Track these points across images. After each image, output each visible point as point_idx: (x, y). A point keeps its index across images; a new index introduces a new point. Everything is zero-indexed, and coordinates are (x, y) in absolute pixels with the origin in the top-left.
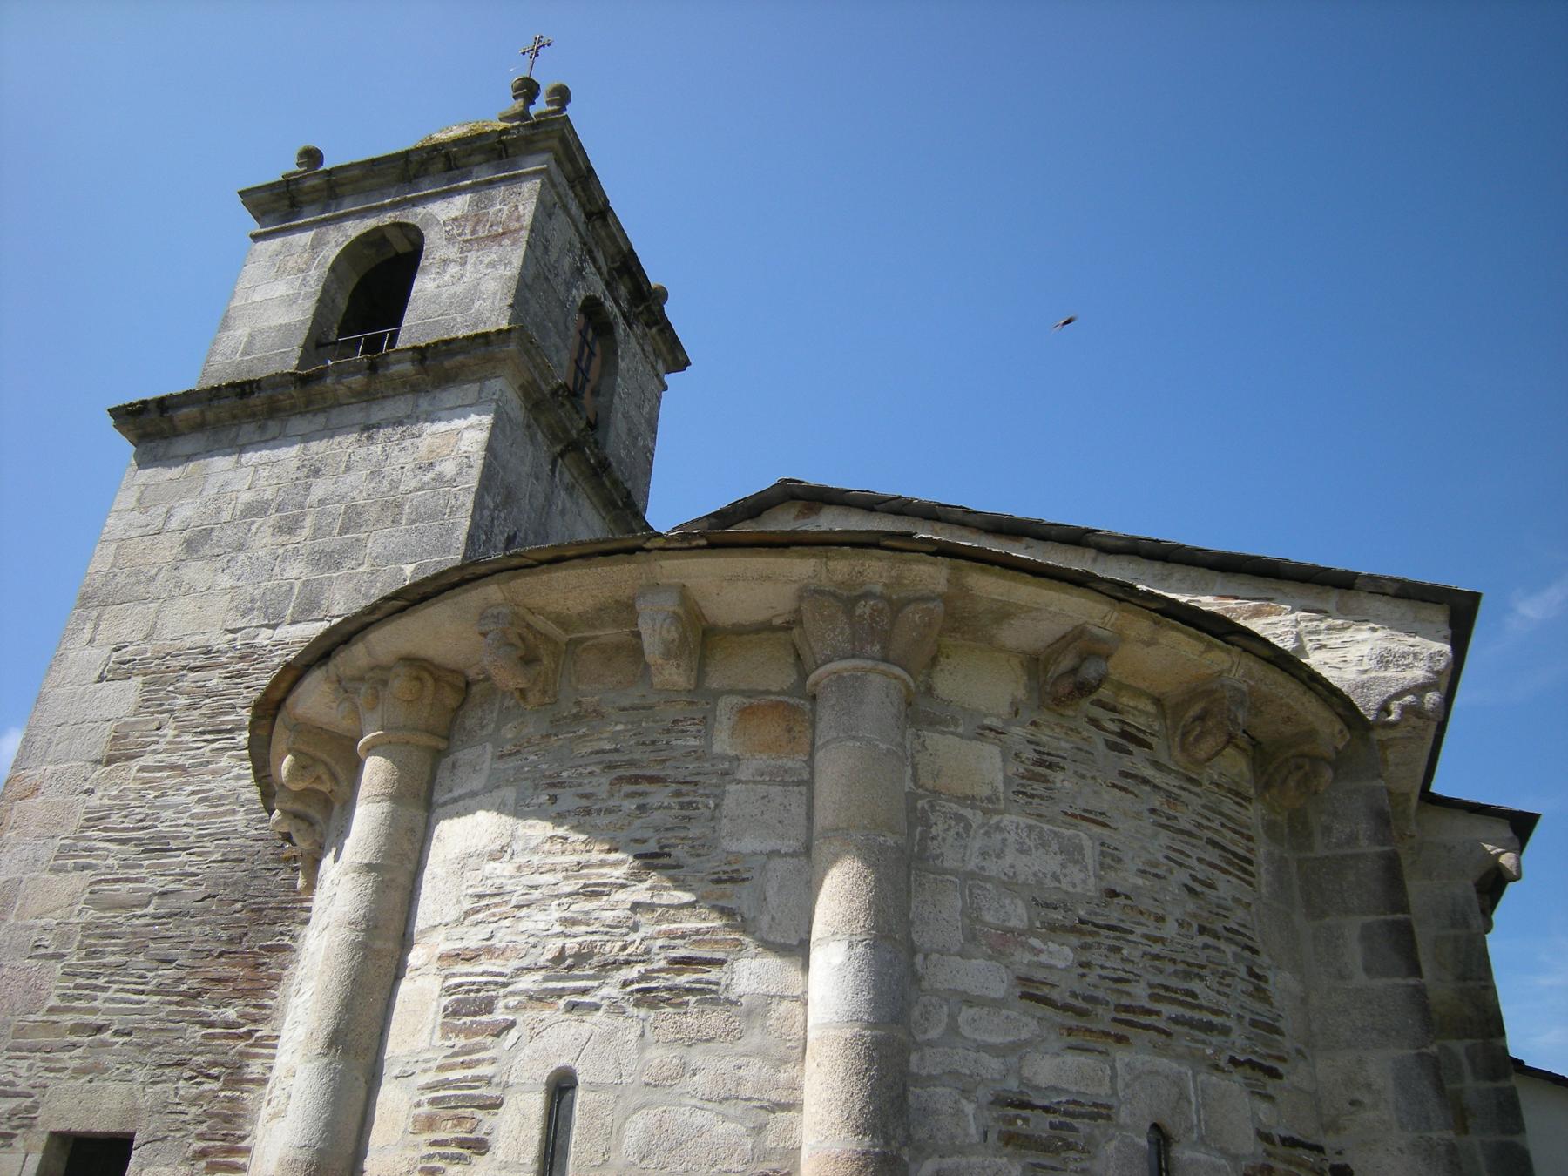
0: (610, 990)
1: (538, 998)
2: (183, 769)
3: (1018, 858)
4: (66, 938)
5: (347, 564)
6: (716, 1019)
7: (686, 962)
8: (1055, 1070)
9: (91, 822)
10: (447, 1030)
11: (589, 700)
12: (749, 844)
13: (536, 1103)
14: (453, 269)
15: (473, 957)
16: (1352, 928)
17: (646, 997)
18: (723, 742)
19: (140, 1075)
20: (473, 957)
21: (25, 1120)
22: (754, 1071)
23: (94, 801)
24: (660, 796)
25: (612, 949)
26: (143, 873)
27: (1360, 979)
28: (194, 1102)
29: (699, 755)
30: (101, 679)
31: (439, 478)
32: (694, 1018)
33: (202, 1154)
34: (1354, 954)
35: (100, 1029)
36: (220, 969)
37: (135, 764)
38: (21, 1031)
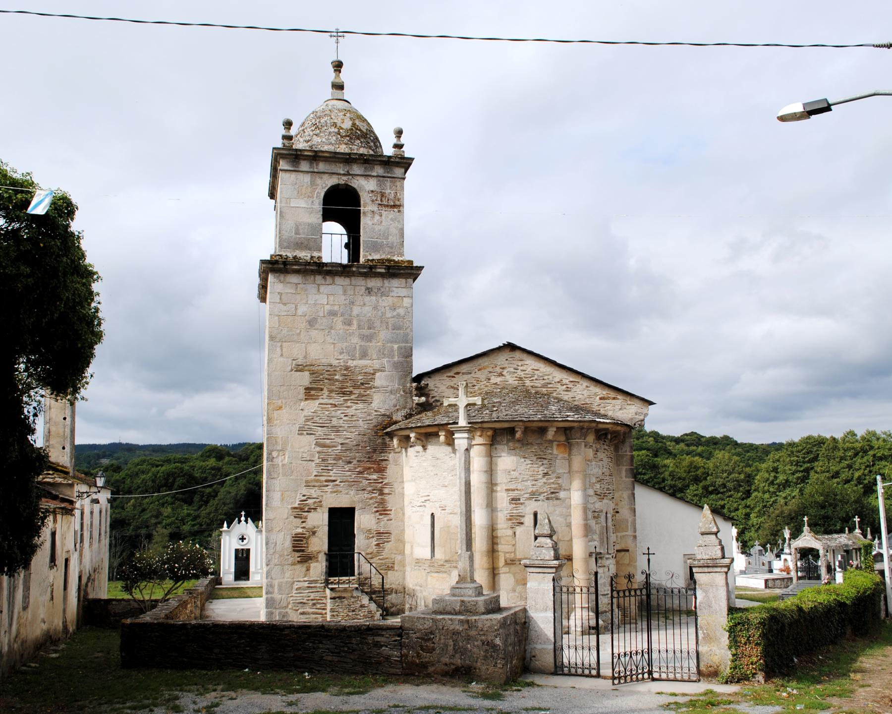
0: (541, 497)
1: (530, 499)
2: (335, 406)
3: (596, 470)
4: (313, 456)
5: (374, 341)
6: (558, 502)
7: (553, 493)
8: (598, 505)
9: (307, 420)
10: (510, 503)
11: (530, 441)
12: (561, 471)
13: (532, 517)
14: (377, 217)
15: (513, 490)
16: (624, 468)
17: (548, 499)
18: (555, 452)
19: (352, 493)
20: (513, 490)
21: (320, 504)
22: (564, 510)
23: (305, 413)
24: (545, 462)
25: (541, 490)
26: (333, 437)
27: (624, 479)
28: (371, 498)
29: (551, 454)
30: (292, 370)
31: (398, 315)
32: (556, 502)
33: (377, 511)
34: (624, 473)
35: (334, 481)
36: (368, 465)
37: (317, 402)
38: (307, 482)
